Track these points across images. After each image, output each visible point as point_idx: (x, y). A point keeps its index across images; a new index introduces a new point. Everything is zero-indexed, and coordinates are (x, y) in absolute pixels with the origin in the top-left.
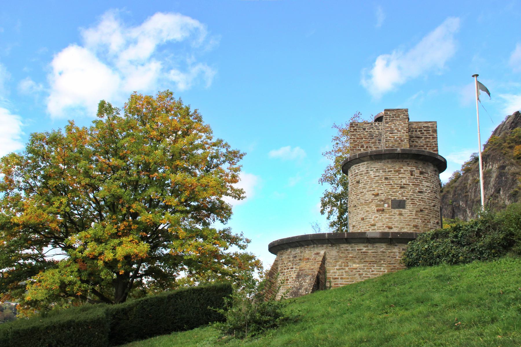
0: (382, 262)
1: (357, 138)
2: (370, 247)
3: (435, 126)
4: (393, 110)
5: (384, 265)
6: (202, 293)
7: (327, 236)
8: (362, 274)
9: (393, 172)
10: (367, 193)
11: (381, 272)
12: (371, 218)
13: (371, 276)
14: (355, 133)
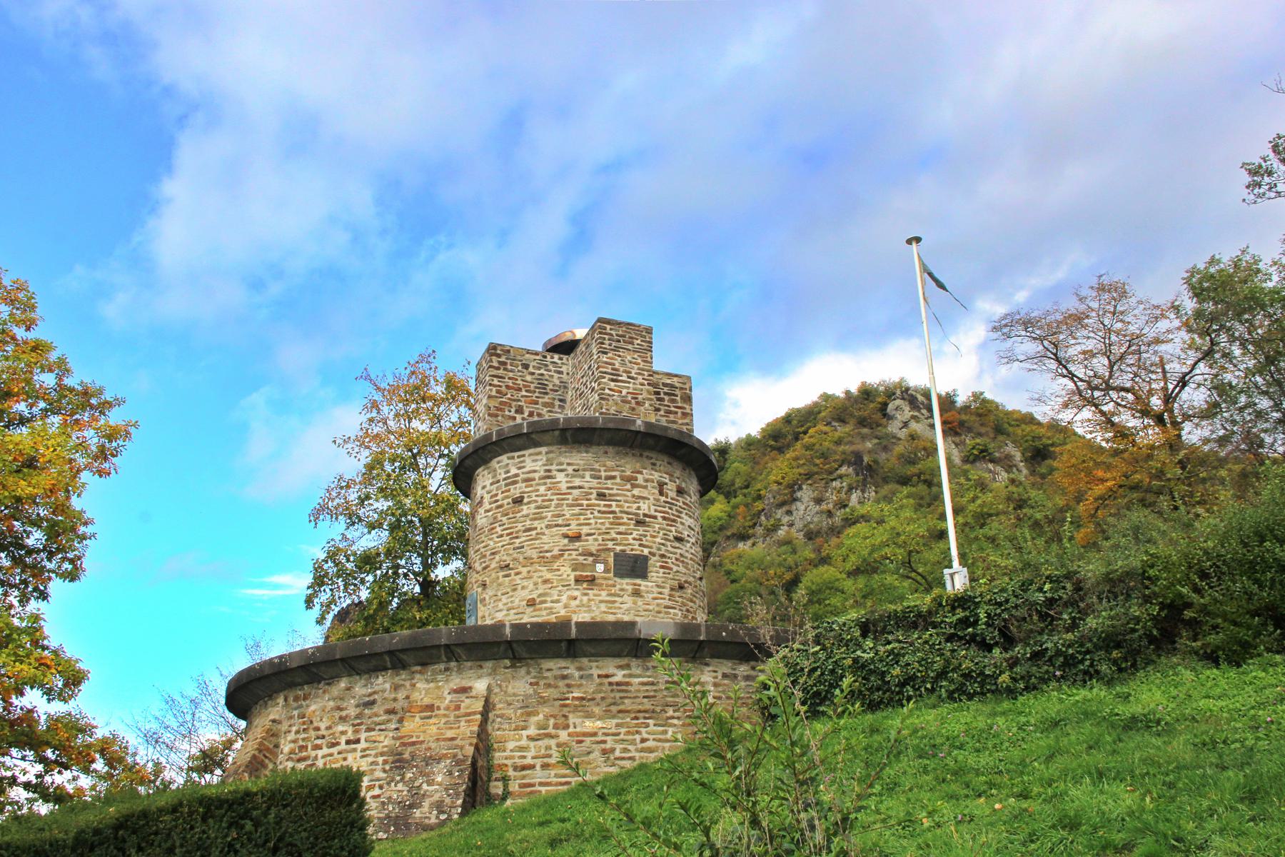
0: (670, 713)
1: (508, 387)
2: (636, 666)
3: (687, 386)
4: (619, 324)
5: (675, 721)
6: (246, 815)
7: (508, 630)
8: (613, 750)
9: (618, 480)
10: (547, 532)
11: (668, 741)
12: (558, 601)
13: (637, 755)
14: (501, 372)
